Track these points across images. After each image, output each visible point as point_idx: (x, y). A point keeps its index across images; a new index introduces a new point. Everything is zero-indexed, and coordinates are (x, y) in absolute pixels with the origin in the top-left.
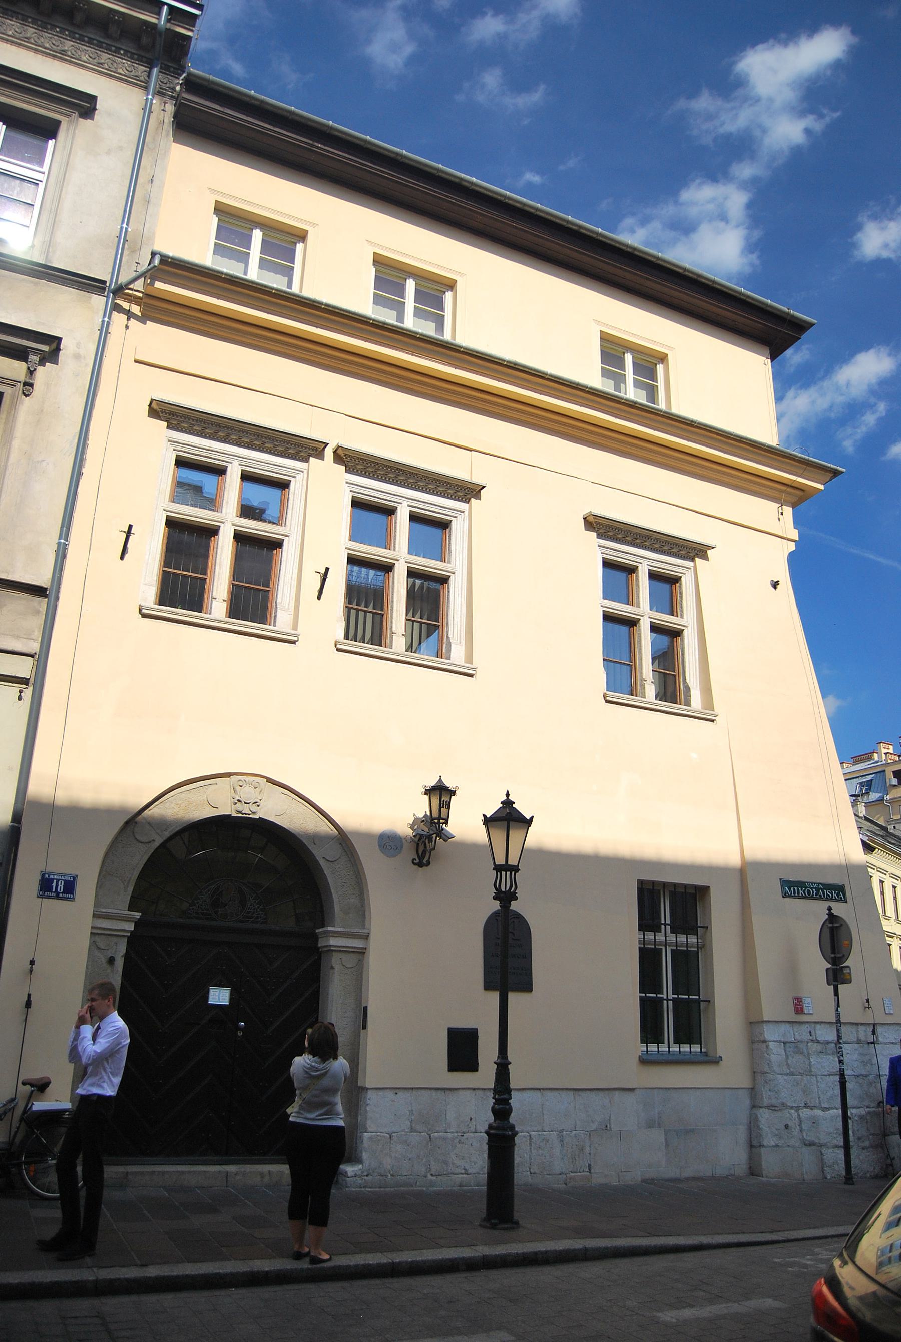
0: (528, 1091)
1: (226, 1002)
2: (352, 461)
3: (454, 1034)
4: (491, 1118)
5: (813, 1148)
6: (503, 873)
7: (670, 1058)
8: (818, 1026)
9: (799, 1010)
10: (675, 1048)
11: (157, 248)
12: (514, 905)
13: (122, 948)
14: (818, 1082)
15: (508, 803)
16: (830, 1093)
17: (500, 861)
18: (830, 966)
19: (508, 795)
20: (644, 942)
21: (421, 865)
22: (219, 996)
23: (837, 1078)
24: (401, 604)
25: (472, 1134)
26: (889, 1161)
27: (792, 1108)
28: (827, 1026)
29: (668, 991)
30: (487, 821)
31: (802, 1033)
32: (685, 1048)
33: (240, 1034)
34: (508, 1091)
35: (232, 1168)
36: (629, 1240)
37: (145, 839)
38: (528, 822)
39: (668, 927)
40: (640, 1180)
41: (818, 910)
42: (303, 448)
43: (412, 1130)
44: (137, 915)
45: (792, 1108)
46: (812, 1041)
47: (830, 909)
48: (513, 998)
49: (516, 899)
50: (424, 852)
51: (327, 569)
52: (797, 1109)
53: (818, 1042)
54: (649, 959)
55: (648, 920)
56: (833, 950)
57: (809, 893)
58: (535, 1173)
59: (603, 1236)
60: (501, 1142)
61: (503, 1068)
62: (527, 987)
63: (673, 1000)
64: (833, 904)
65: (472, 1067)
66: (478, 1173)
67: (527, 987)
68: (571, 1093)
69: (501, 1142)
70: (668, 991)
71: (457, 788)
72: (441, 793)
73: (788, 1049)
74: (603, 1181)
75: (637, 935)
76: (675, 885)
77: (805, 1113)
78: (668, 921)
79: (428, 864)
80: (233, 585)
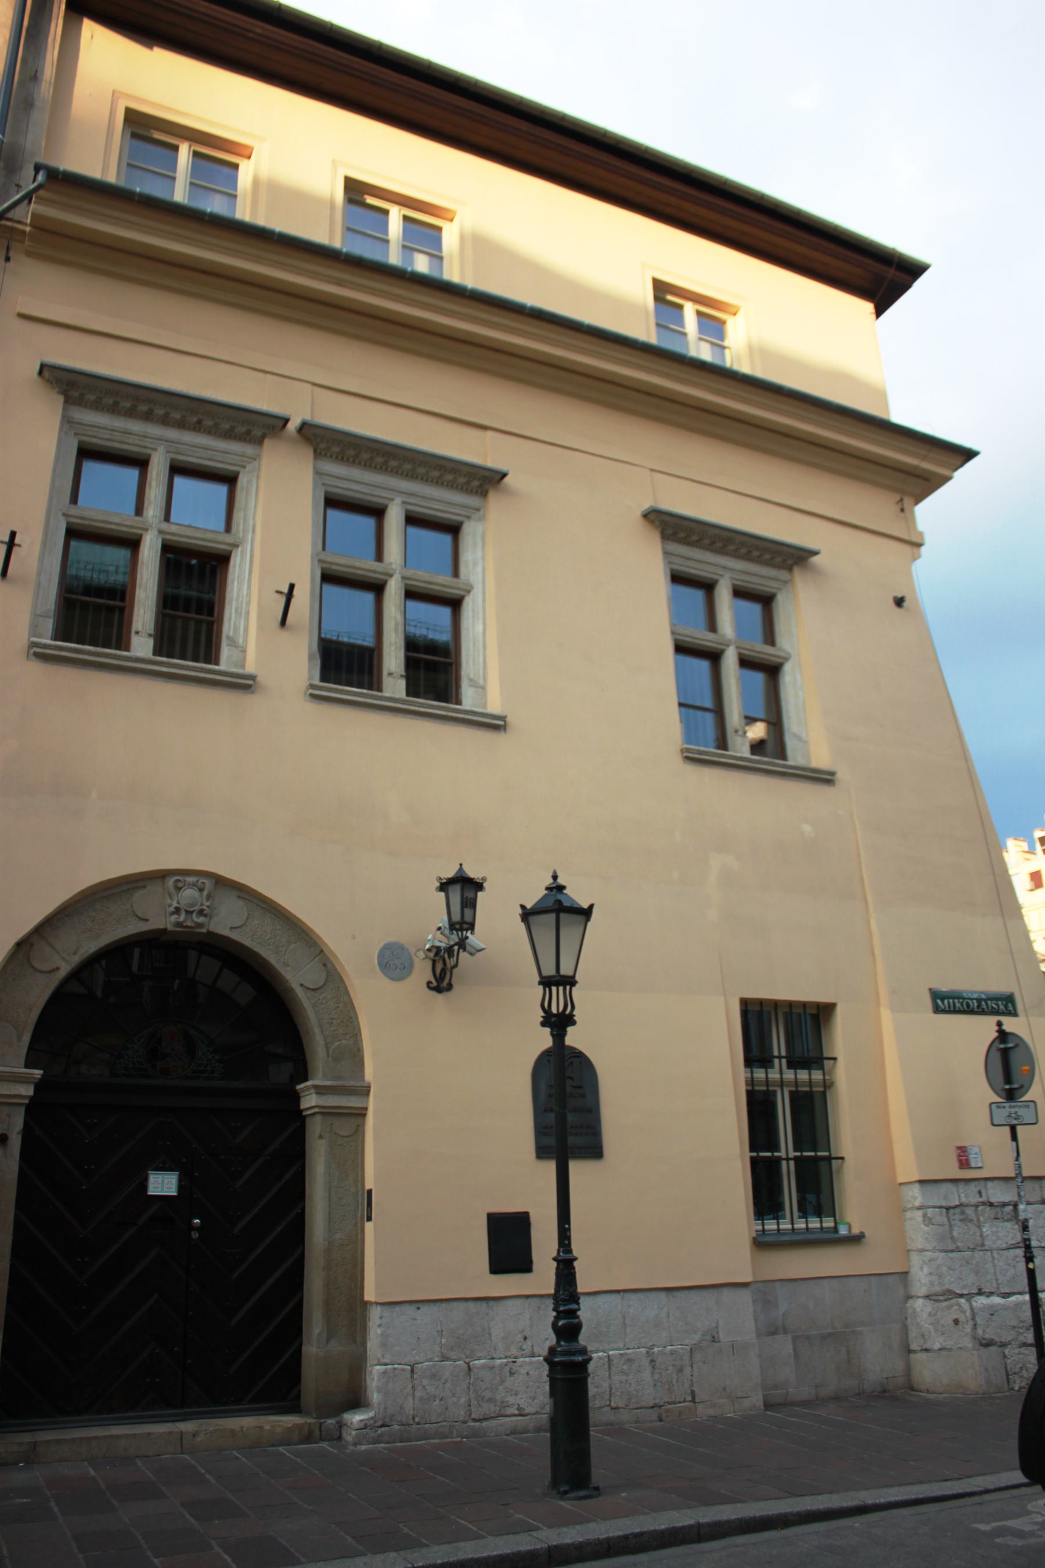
0: (603, 1296)
1: (173, 1192)
2: (322, 441)
3: (757, 1019)
4: (552, 1339)
5: (993, 1348)
6: (554, 989)
7: (795, 1238)
8: (990, 1184)
9: (964, 1163)
10: (800, 1225)
11: (41, 159)
12: (573, 1038)
13: (18, 1121)
14: (993, 1258)
16: (1011, 1272)
17: (549, 970)
19: (555, 877)
20: (751, 1082)
21: (438, 990)
22: (163, 1184)
23: (1020, 1252)
25: (527, 1359)
27: (961, 1296)
28: (1001, 1183)
29: (786, 1147)
30: (527, 915)
31: (968, 1195)
32: (814, 1223)
33: (195, 1235)
34: (574, 1297)
35: (187, 1427)
36: (761, 1504)
37: (46, 967)
38: (586, 913)
39: (784, 1061)
40: (757, 1400)
42: (256, 427)
43: (445, 1358)
44: (38, 1073)
45: (961, 1296)
46: (984, 1203)
47: (999, 1024)
48: (577, 1169)
49: (574, 1023)
50: (443, 971)
51: (292, 587)
52: (969, 1297)
53: (991, 1205)
54: (759, 1108)
55: (755, 1054)
56: (1008, 1078)
57: (968, 1005)
58: (617, 1408)
60: (569, 1374)
61: (566, 1268)
62: (594, 1151)
63: (796, 1159)
64: (1004, 1019)
65: (524, 1265)
66: (537, 1413)
67: (594, 1151)
68: (662, 1295)
69: (569, 1374)
70: (786, 1147)
71: (484, 879)
72: (464, 888)
73: (952, 1218)
74: (711, 1412)
75: (742, 1073)
76: (790, 1004)
77: (981, 1301)
78: (783, 1053)
79: (450, 987)
80: (164, 615)
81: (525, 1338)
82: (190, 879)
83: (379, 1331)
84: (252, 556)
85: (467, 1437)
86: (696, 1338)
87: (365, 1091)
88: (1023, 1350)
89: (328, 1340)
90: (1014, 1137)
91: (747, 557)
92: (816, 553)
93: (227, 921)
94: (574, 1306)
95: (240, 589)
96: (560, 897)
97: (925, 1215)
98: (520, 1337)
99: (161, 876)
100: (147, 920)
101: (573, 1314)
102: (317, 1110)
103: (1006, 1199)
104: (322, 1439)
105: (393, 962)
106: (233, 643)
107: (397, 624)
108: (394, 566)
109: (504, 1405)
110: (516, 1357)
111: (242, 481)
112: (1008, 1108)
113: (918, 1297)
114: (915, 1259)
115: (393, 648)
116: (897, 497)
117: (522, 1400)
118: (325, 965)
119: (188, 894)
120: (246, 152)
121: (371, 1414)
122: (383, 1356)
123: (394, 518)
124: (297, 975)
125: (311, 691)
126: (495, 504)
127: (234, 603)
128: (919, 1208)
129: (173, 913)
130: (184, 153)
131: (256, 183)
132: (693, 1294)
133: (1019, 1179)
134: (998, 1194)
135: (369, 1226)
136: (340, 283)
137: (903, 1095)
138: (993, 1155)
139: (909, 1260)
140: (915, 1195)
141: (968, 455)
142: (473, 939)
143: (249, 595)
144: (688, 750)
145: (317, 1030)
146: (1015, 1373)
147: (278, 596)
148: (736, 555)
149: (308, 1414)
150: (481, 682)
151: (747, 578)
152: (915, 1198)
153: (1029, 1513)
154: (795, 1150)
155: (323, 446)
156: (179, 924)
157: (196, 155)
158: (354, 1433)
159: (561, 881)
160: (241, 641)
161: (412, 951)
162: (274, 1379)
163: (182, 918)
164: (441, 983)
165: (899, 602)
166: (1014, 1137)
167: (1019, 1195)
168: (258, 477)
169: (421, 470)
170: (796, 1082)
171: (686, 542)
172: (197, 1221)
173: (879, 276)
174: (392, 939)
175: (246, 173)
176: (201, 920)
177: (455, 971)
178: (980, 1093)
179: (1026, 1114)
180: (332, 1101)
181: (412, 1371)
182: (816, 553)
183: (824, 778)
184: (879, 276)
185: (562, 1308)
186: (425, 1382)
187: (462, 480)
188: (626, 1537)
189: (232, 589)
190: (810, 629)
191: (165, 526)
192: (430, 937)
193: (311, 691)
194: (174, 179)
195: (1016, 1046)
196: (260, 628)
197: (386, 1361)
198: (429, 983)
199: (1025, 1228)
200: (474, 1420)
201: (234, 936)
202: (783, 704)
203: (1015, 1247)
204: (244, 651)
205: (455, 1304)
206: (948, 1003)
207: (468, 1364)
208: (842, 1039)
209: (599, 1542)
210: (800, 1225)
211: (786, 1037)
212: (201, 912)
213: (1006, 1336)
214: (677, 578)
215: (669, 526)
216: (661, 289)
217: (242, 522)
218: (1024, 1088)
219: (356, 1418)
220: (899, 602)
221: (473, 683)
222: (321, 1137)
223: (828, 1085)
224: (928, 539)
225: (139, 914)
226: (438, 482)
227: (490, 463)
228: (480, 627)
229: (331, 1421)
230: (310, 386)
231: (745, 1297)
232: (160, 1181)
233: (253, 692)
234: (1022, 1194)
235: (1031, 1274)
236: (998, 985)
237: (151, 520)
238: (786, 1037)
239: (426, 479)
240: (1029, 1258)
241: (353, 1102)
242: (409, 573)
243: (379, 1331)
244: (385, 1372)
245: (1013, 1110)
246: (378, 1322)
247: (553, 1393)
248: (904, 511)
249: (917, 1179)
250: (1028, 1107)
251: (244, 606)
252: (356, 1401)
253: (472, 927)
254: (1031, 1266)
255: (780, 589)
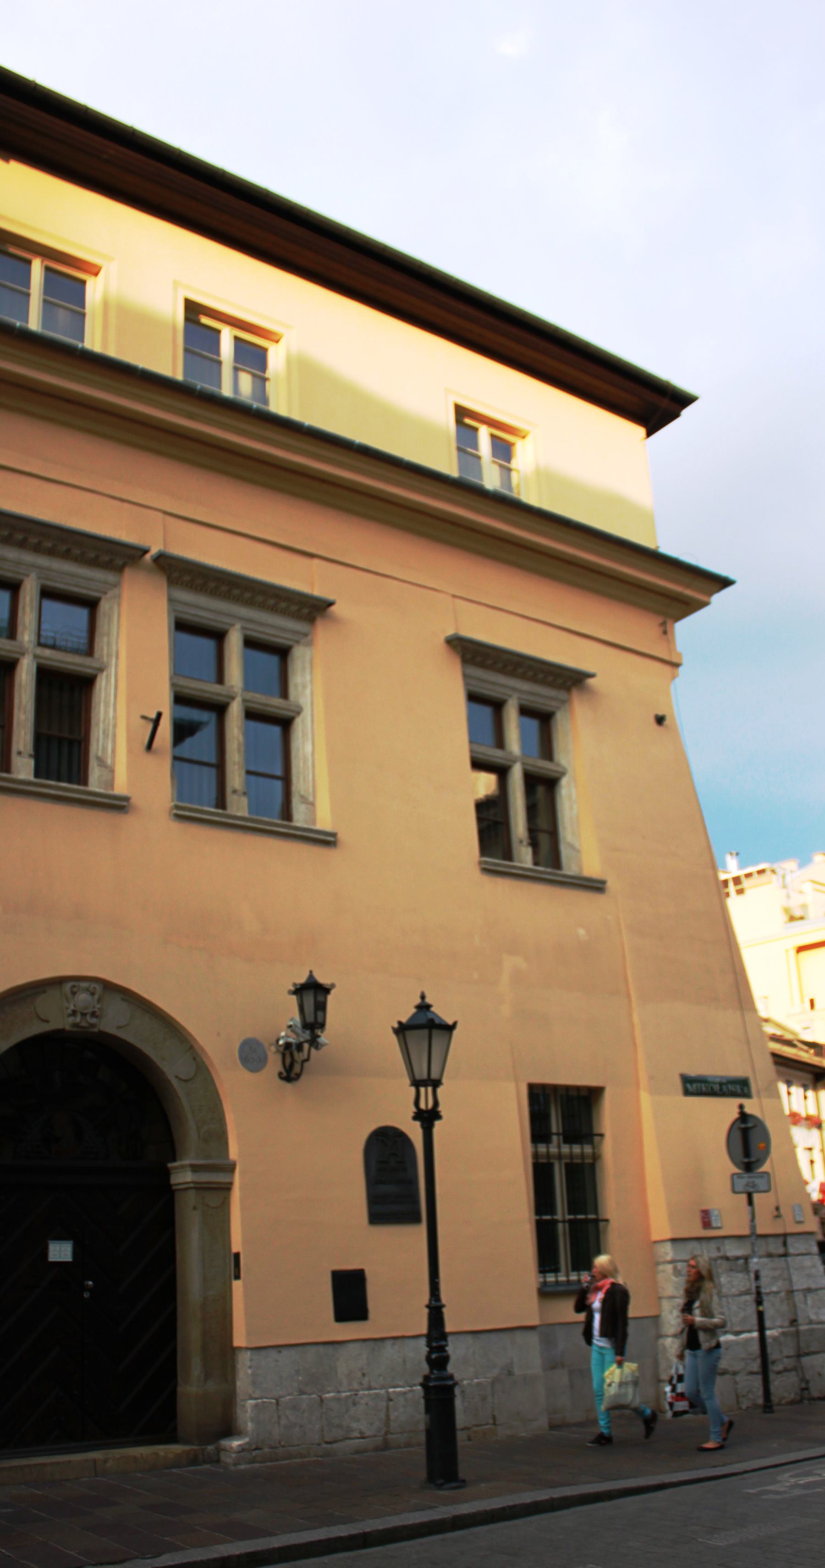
2: (177, 571)
4: (425, 1368)
5: (727, 1376)
6: (422, 1090)
8: (727, 1241)
9: (707, 1223)
15: (424, 1007)
16: (742, 1314)
18: (737, 1170)
19: (423, 997)
20: (536, 1155)
22: (60, 1251)
24: (234, 752)
25: (366, 1392)
26: (803, 1385)
29: (561, 1212)
30: (402, 1030)
33: (86, 1295)
34: (444, 1336)
38: (449, 1029)
40: (543, 1422)
41: (725, 1110)
42: (117, 557)
43: (302, 1392)
47: (741, 1107)
53: (727, 1258)
54: (542, 1174)
55: (539, 1132)
56: (747, 1152)
59: (553, 1485)
60: (439, 1394)
64: (745, 1101)
66: (375, 1436)
68: (469, 1339)
69: (439, 1394)
70: (561, 1212)
71: (333, 986)
76: (567, 1088)
79: (298, 1076)
81: (364, 1375)
82: (84, 985)
83: (249, 1371)
84: (116, 681)
85: (321, 1456)
86: (495, 1372)
87: (230, 1168)
88: (750, 1377)
89: (206, 1380)
90: (750, 1202)
91: (534, 680)
92: (592, 676)
93: (114, 1021)
94: (443, 1343)
95: (106, 712)
96: (430, 1016)
97: (675, 1269)
98: (359, 1374)
99: (58, 982)
100: (47, 1021)
101: (442, 1349)
102: (192, 1185)
103: (739, 1252)
104: (205, 1462)
105: (251, 1055)
106: (101, 762)
107: (239, 744)
108: (235, 689)
109: (350, 1430)
110: (357, 1391)
111: (104, 606)
112: (746, 1179)
113: (667, 1336)
114: (666, 1305)
115: (237, 767)
116: (660, 620)
117: (363, 1426)
118: (194, 1059)
119: (83, 998)
120: (94, 270)
121: (247, 1440)
122: (254, 1392)
123: (234, 642)
124: (172, 1067)
125: (175, 811)
126: (322, 632)
127: (101, 725)
128: (671, 1262)
129: (70, 1015)
130: (37, 268)
131: (106, 304)
132: (493, 1336)
133: (754, 1237)
134: (733, 1250)
135: (237, 1286)
136: (191, 416)
137: (659, 1168)
138: (732, 1217)
139: (659, 1306)
140: (668, 1251)
141: (724, 583)
142: (324, 1038)
143: (115, 718)
144: (486, 863)
145: (189, 1116)
146: (744, 1396)
147: (143, 722)
148: (523, 677)
149: (186, 1442)
150: (311, 799)
151: (532, 698)
152: (667, 1254)
153: (780, 1482)
154: (570, 1213)
155: (176, 575)
156: (76, 1025)
157: (48, 269)
158: (234, 1455)
159: (428, 1000)
160: (109, 761)
161: (266, 1045)
162: (155, 1416)
163: (78, 1019)
164: (289, 1075)
165: (660, 720)
166: (750, 1202)
167: (753, 1251)
168: (119, 605)
169: (260, 598)
170: (571, 1156)
171: (482, 665)
172: (90, 1283)
173: (650, 402)
174: (249, 1035)
175: (95, 291)
176: (94, 1021)
177: (306, 1064)
178: (721, 1166)
179: (761, 1183)
180: (205, 1177)
181: (278, 1404)
182: (592, 676)
183: (596, 886)
184: (650, 402)
185: (434, 1344)
186: (288, 1412)
187: (294, 608)
188: (504, 1509)
189: (99, 712)
190: (589, 754)
191: (40, 651)
192: (283, 1034)
193: (175, 811)
194: (28, 295)
195: (755, 1126)
196: (130, 751)
197: (256, 1395)
198: (280, 1074)
199: (757, 1277)
200: (327, 1443)
201: (121, 1034)
202: (559, 815)
203: (747, 1293)
204: (112, 771)
205: (309, 1347)
206: (696, 1086)
207: (320, 1397)
208: (609, 1118)
209: (486, 1513)
210: (574, 1277)
211: (564, 1116)
212: (93, 1014)
213: (738, 1366)
214: (473, 698)
215: (469, 652)
216: (461, 412)
217: (105, 648)
218: (760, 1161)
219: (236, 1443)
220: (660, 720)
221: (304, 799)
222: (195, 1208)
223: (596, 1157)
224: (685, 661)
225: (42, 1017)
226: (273, 609)
227: (317, 592)
228: (308, 748)
229: (210, 1448)
230: (160, 515)
231: (533, 1339)
232: (58, 1249)
233: (127, 812)
234: (756, 1249)
235: (761, 1315)
236: (736, 1070)
237: (26, 645)
238: (564, 1116)
239: (263, 606)
240: (759, 1302)
241: (220, 1178)
242: (250, 696)
243: (249, 1371)
244: (256, 1405)
245: (751, 1180)
246: (248, 1363)
247: (428, 1409)
248: (666, 632)
249: (669, 1236)
250: (762, 1177)
251: (111, 728)
252: (229, 1429)
253: (322, 1026)
254: (761, 1308)
255: (559, 708)
